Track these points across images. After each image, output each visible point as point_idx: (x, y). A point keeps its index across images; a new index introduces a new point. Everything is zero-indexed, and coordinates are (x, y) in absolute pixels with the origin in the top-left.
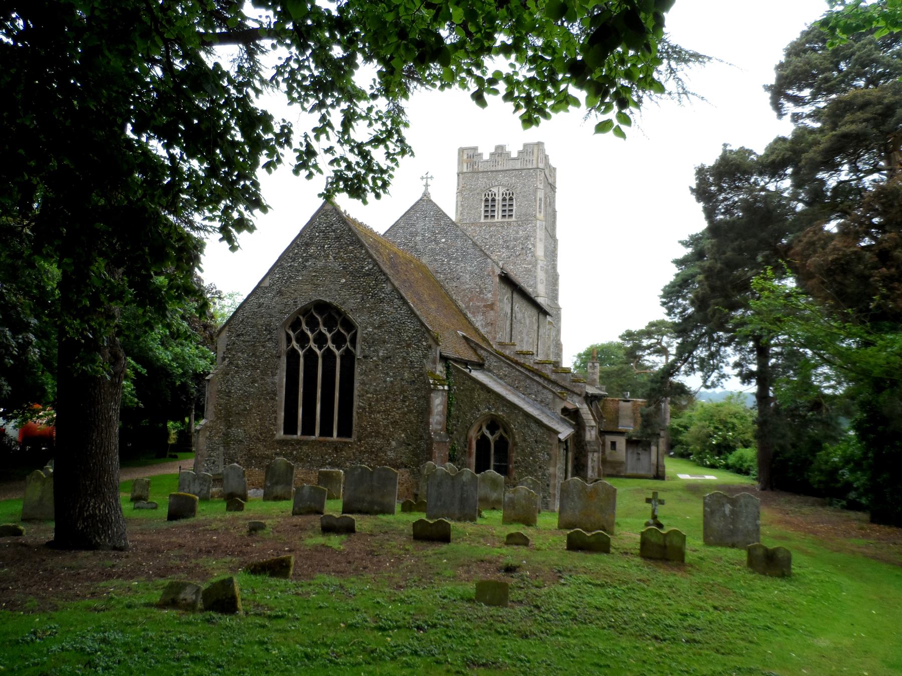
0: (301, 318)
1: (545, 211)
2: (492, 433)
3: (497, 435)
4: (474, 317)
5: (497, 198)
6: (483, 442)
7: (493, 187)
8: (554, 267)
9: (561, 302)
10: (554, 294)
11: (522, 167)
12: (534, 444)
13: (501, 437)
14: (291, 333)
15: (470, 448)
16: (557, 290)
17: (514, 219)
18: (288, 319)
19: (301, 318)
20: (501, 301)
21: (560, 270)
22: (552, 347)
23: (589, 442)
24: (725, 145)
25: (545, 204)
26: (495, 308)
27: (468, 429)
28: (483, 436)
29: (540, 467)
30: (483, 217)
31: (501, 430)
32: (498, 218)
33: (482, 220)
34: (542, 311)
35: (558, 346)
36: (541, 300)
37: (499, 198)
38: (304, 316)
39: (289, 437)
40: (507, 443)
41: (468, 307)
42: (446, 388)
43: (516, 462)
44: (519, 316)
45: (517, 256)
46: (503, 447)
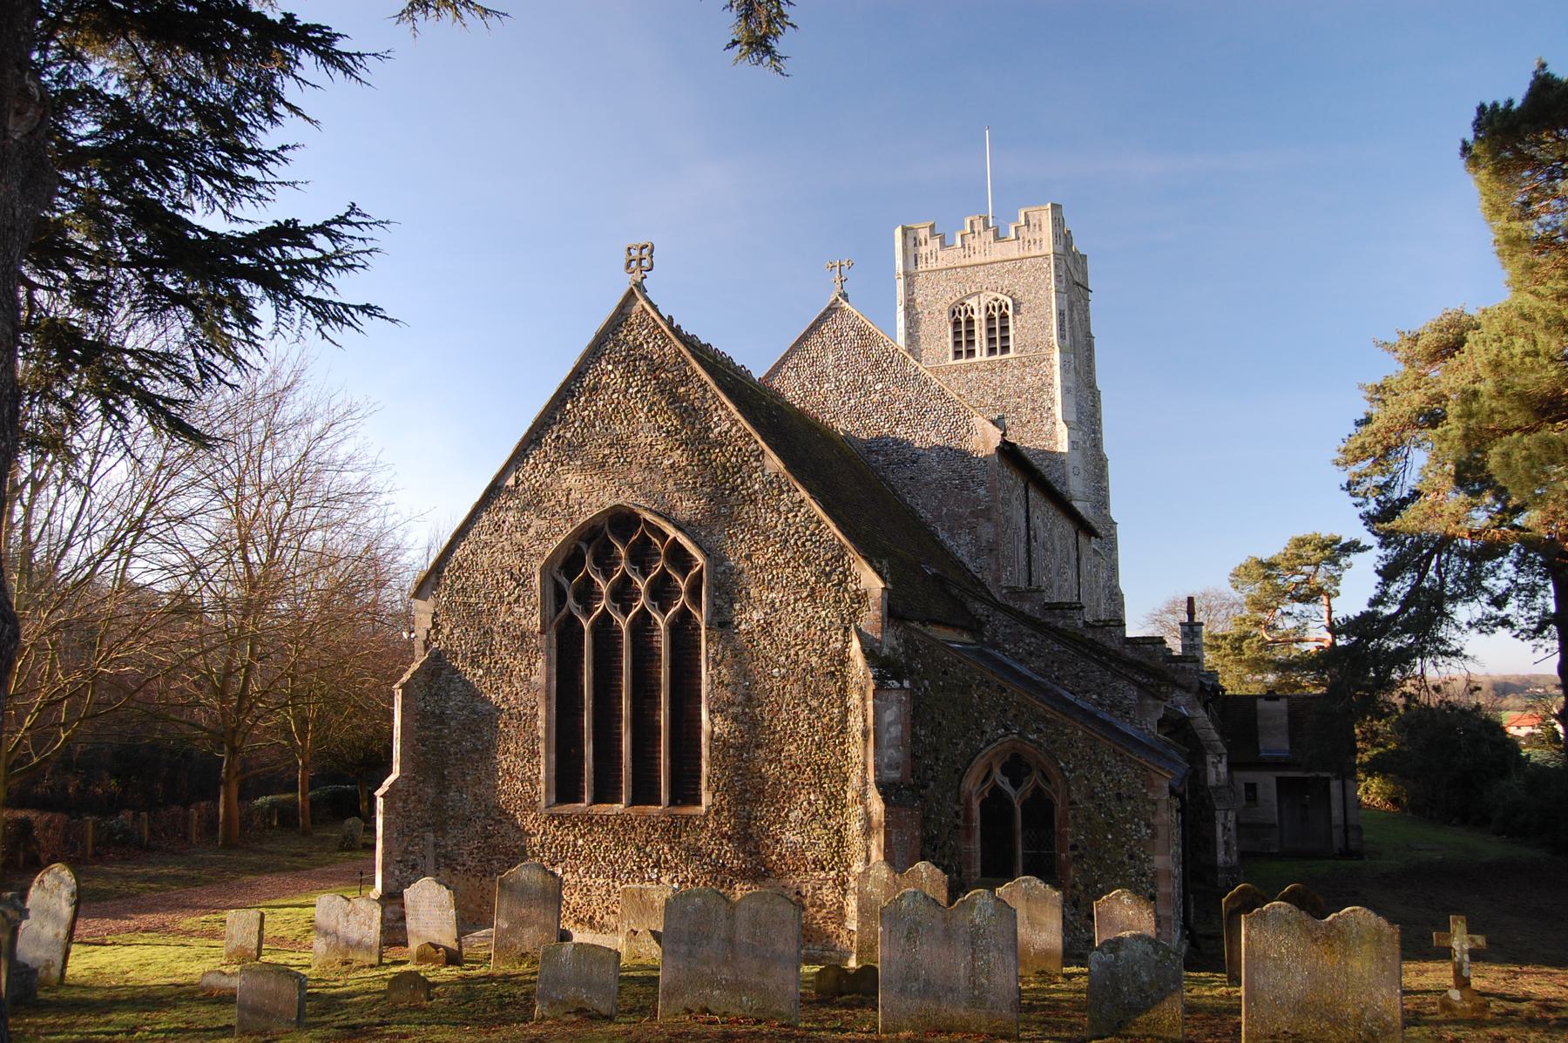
0: (584, 546)
1: (1073, 335)
2: (1016, 784)
3: (1027, 786)
4: (952, 537)
5: (975, 317)
6: (996, 804)
7: (968, 297)
8: (1097, 444)
9: (1115, 512)
10: (1102, 502)
11: (1022, 254)
12: (1113, 804)
13: (1037, 790)
14: (563, 580)
15: (968, 818)
16: (1106, 489)
17: (1012, 354)
18: (556, 551)
19: (584, 546)
20: (1007, 502)
21: (1107, 448)
22: (1103, 601)
23: (1216, 788)
24: (1543, 66)
25: (1071, 320)
26: (995, 516)
27: (961, 774)
28: (996, 791)
29: (1131, 857)
30: (951, 355)
31: (1036, 775)
32: (981, 355)
33: (951, 361)
34: (1084, 528)
35: (1116, 598)
36: (1079, 505)
37: (979, 317)
38: (589, 542)
39: (567, 809)
40: (1050, 805)
41: (938, 518)
42: (906, 684)
43: (1074, 847)
44: (1042, 534)
45: (1024, 426)
46: (1040, 811)
